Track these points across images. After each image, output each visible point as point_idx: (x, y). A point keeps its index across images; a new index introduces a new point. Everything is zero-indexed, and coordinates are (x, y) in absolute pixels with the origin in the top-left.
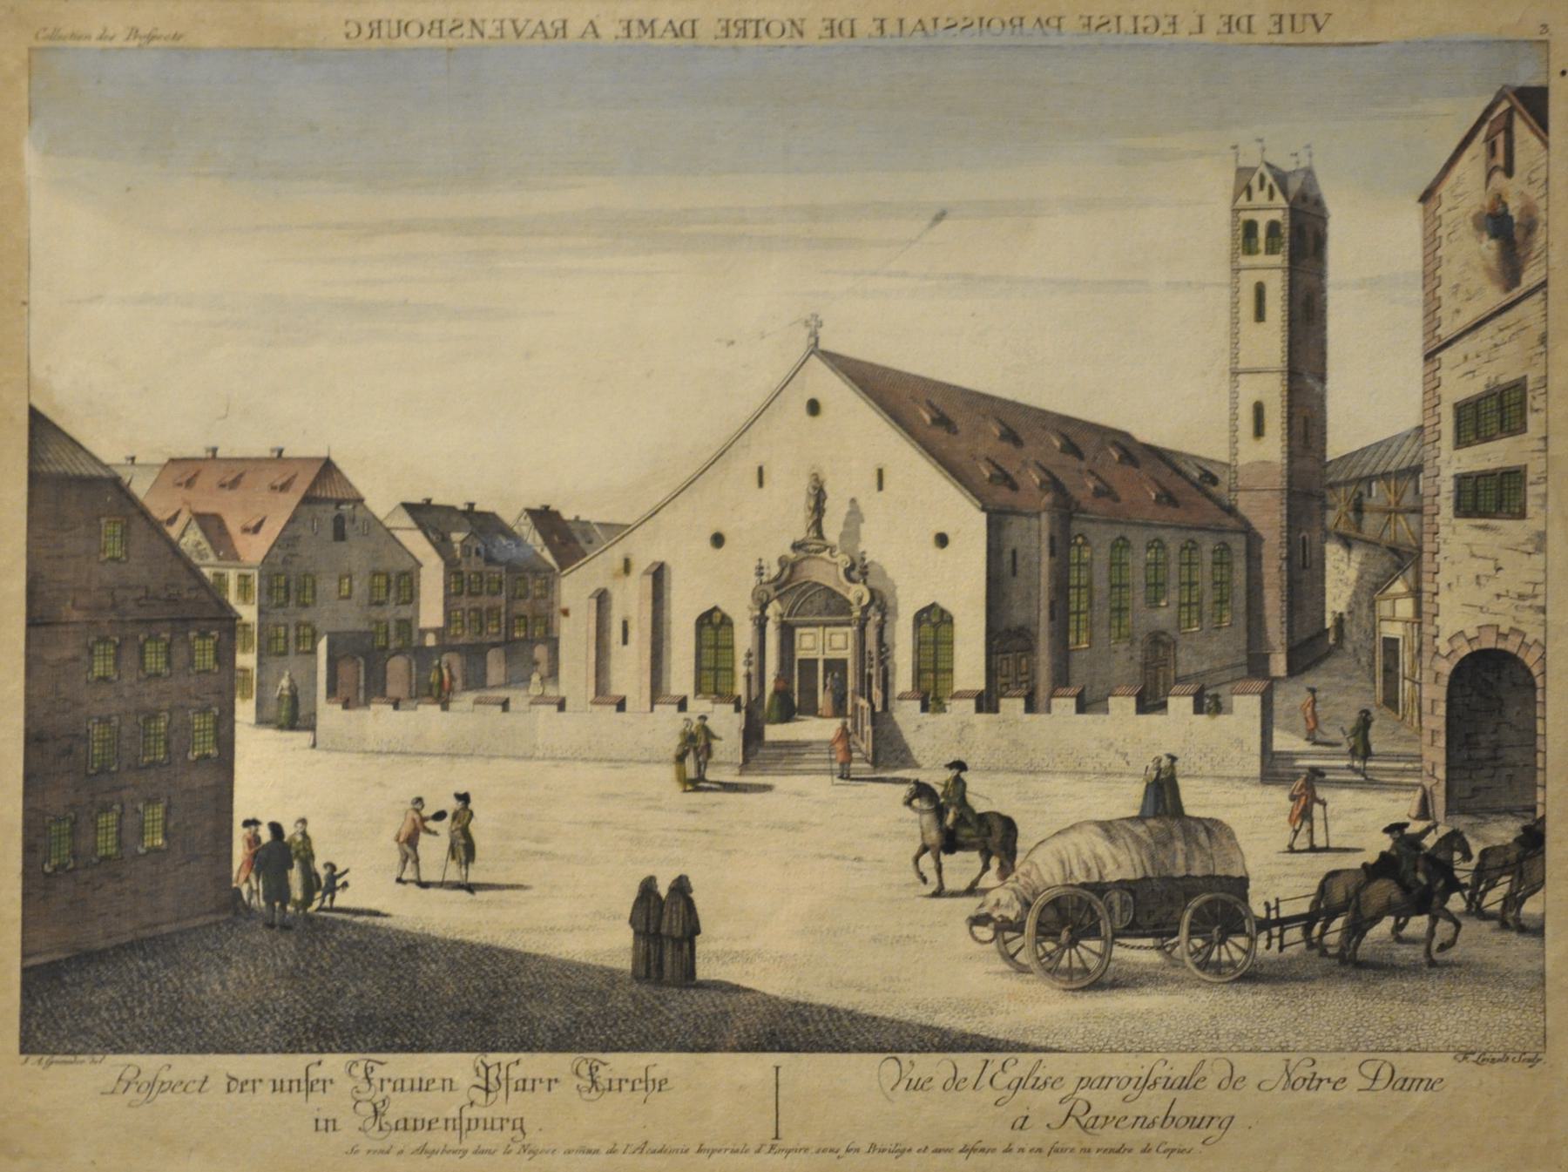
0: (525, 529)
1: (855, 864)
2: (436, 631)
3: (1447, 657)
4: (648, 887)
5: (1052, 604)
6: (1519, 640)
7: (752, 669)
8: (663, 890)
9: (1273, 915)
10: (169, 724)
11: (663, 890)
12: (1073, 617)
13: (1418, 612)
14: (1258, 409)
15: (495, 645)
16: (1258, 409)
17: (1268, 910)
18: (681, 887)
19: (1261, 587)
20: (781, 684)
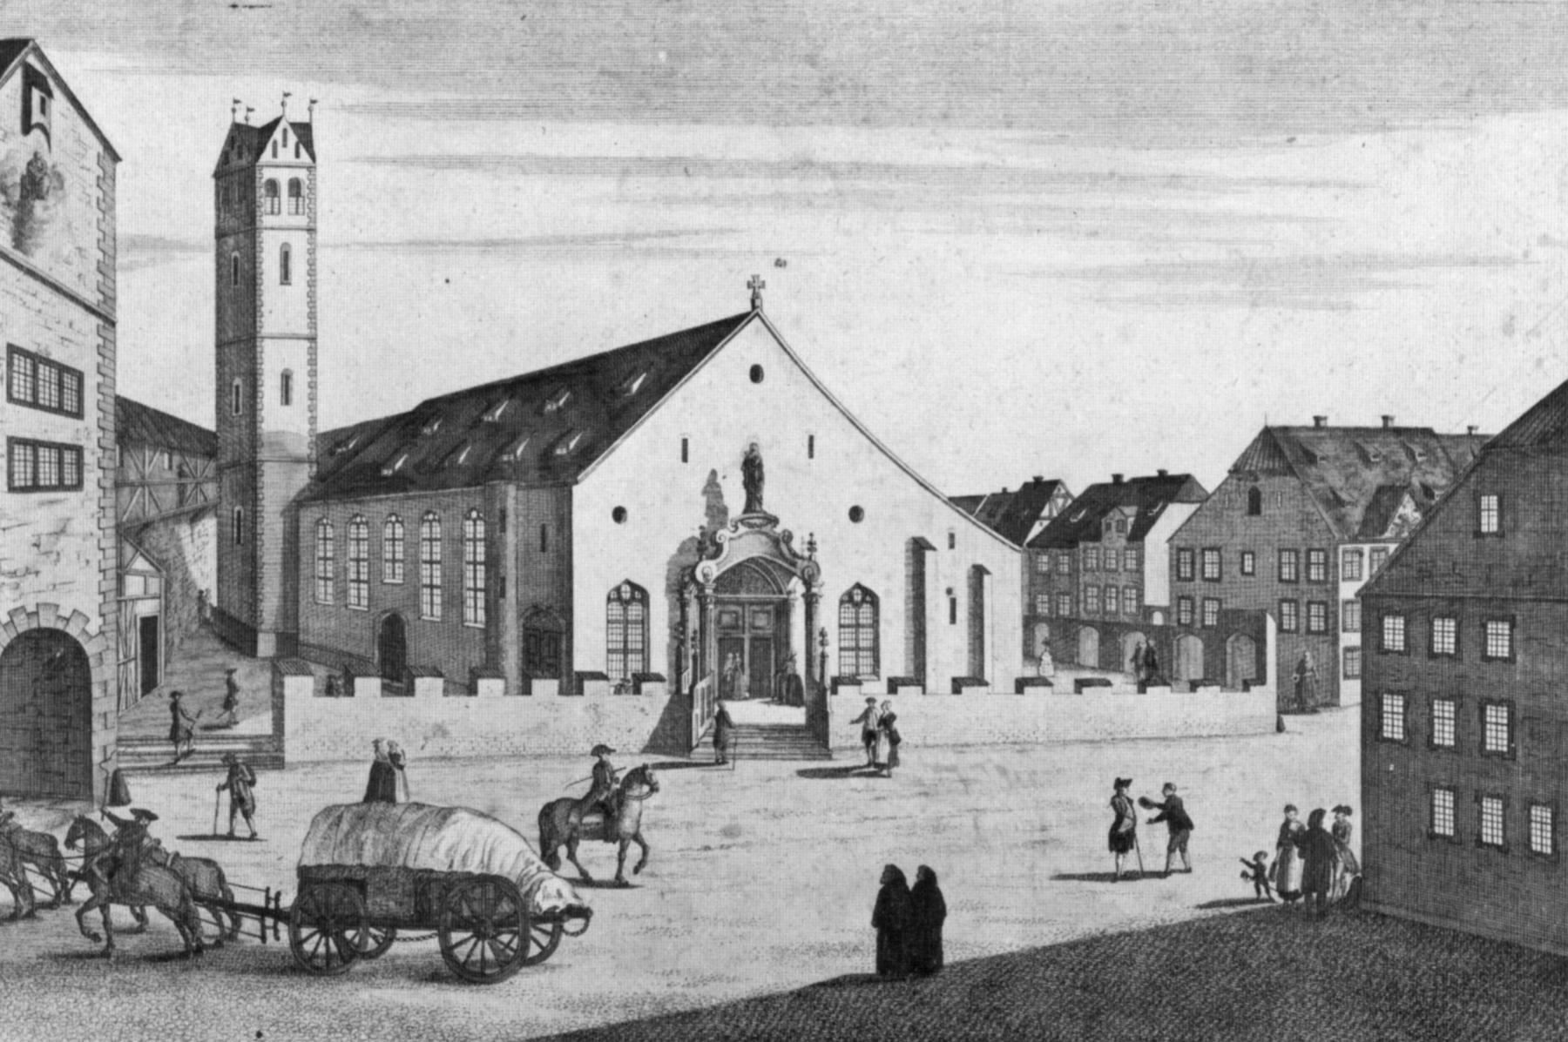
0: (1060, 501)
1: (704, 854)
2: (1166, 611)
3: (59, 617)
4: (893, 876)
5: (503, 594)
6: (23, 616)
7: (819, 649)
8: (911, 881)
9: (272, 905)
10: (165, 909)
11: (911, 881)
12: (481, 584)
13: (120, 579)
14: (286, 399)
15: (1091, 623)
16: (286, 399)
17: (268, 899)
18: (928, 877)
19: (285, 565)
20: (1380, 259)
